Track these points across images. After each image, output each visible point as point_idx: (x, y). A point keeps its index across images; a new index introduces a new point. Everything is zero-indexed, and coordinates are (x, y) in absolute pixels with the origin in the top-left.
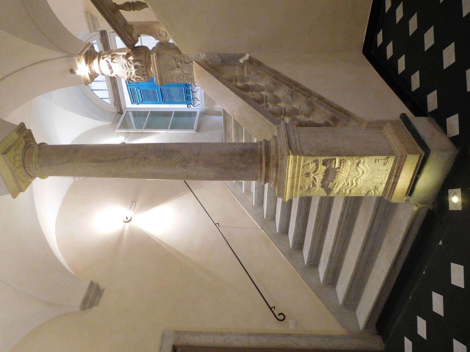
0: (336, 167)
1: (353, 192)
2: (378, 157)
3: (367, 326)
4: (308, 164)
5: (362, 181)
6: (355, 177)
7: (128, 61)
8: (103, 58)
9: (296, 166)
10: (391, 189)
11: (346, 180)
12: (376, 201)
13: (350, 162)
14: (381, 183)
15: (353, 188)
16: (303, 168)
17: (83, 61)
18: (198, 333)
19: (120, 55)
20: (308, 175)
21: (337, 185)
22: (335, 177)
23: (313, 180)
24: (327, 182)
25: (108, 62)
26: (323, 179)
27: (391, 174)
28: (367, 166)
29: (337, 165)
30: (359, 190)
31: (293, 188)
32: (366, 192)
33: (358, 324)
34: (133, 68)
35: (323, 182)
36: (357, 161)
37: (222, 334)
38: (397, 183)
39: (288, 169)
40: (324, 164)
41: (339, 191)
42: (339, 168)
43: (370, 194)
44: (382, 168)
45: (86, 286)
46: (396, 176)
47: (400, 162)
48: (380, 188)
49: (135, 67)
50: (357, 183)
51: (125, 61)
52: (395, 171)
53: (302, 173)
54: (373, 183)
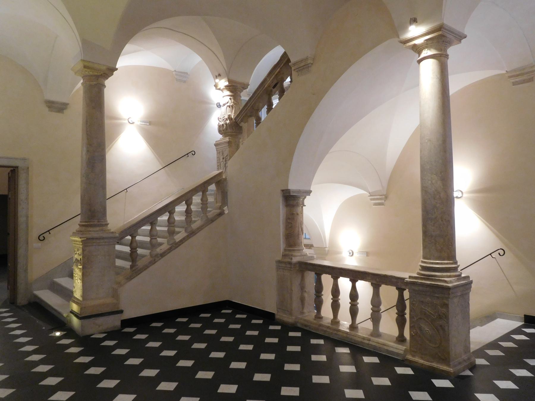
3: (36, 296)
7: (227, 119)
8: (230, 99)
17: (227, 83)
18: (27, 183)
19: (232, 112)
25: (228, 103)
33: (39, 290)
34: (223, 123)
37: (27, 199)
45: (64, 100)
49: (223, 125)
51: (226, 117)
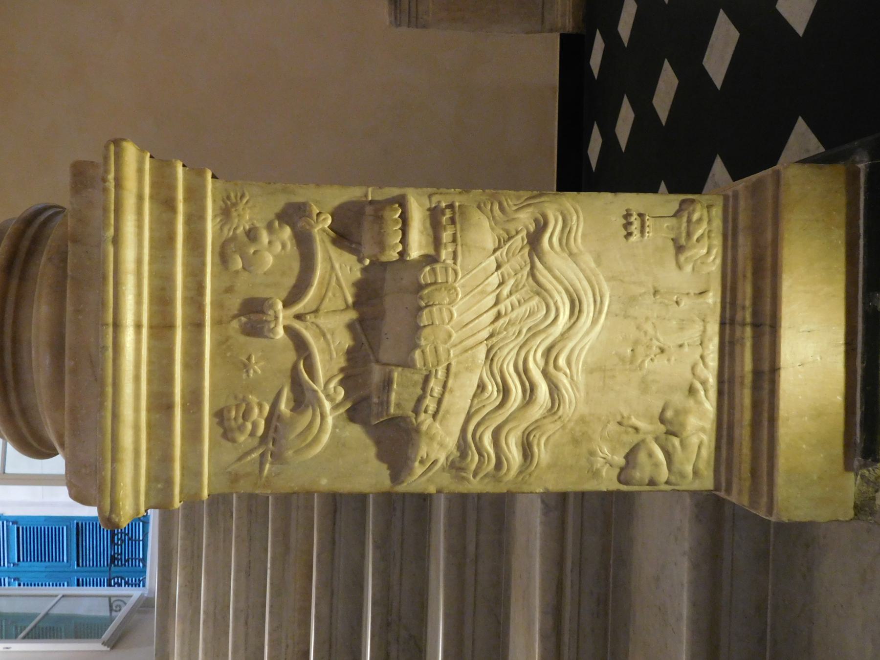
0: (415, 253)
1: (542, 453)
2: (634, 201)
4: (252, 235)
5: (580, 378)
6: (534, 333)
9: (171, 239)
10: (755, 424)
11: (490, 358)
12: (694, 604)
13: (486, 224)
14: (692, 391)
15: (537, 425)
16: (223, 257)
20: (253, 315)
21: (435, 386)
22: (417, 329)
23: (290, 356)
24: (377, 373)
26: (351, 354)
27: (728, 322)
28: (588, 260)
29: (418, 246)
30: (576, 441)
31: (170, 407)
32: (619, 460)
35: (353, 374)
36: (525, 219)
38: (775, 369)
39: (116, 241)
40: (344, 236)
41: (462, 447)
42: (431, 260)
43: (642, 473)
44: (675, 277)
46: (756, 326)
47: (756, 230)
48: (693, 422)
50: (554, 389)
52: (746, 290)
53: (218, 305)
54: (644, 386)
